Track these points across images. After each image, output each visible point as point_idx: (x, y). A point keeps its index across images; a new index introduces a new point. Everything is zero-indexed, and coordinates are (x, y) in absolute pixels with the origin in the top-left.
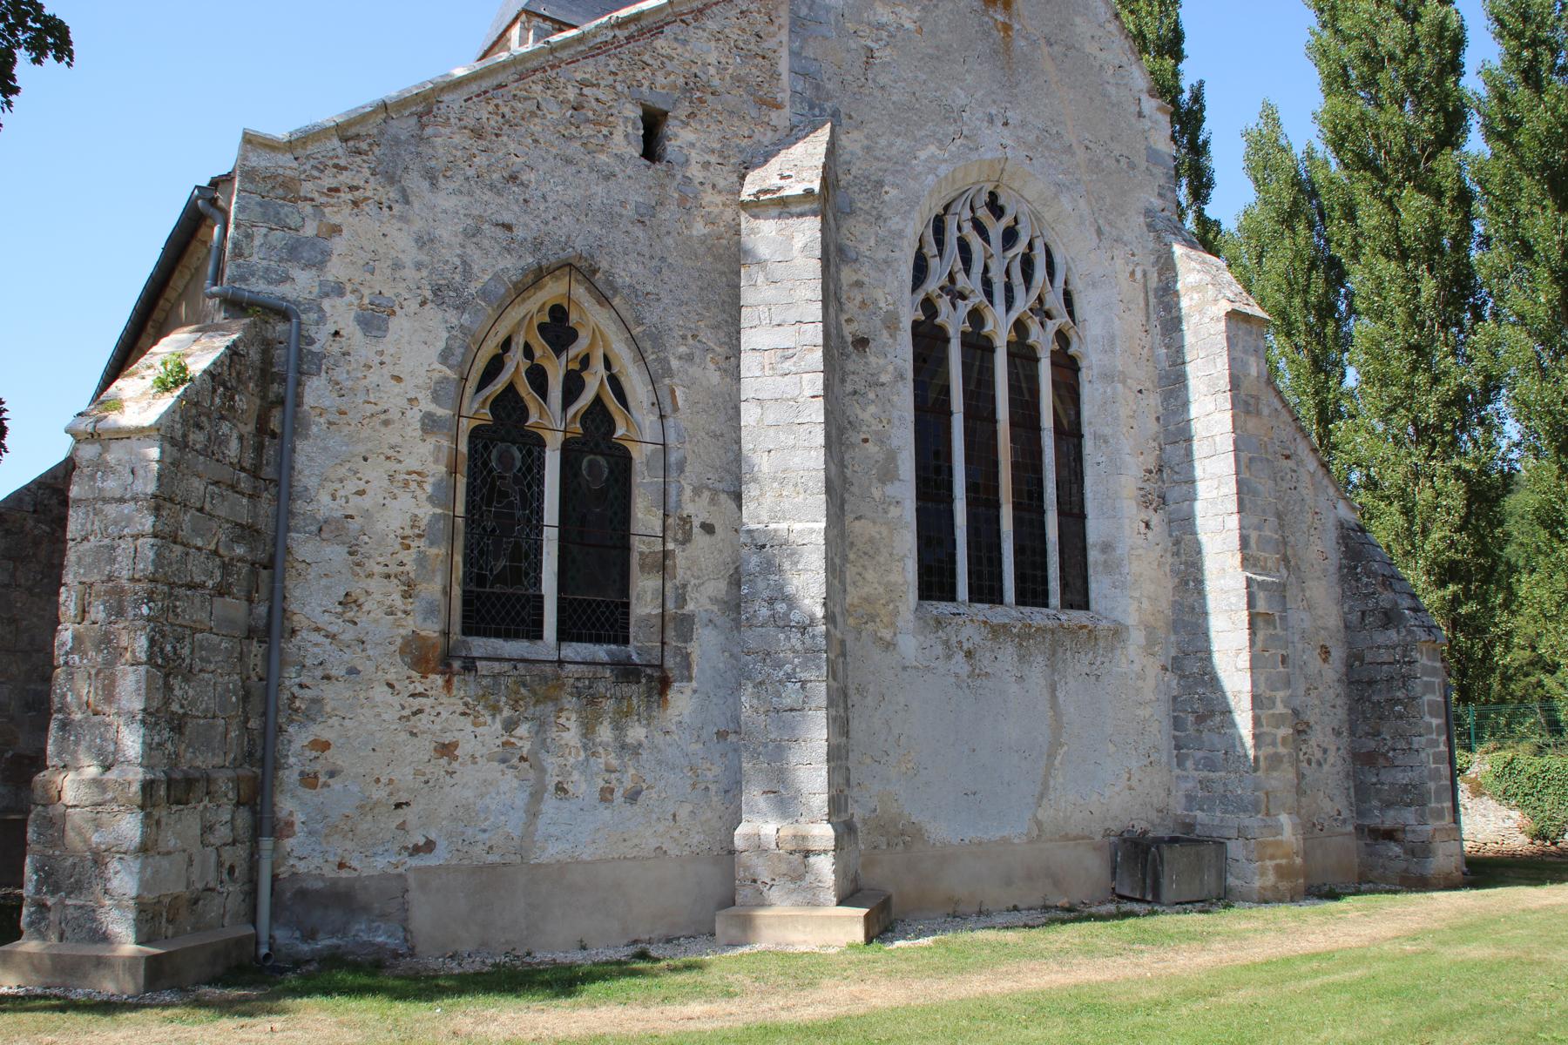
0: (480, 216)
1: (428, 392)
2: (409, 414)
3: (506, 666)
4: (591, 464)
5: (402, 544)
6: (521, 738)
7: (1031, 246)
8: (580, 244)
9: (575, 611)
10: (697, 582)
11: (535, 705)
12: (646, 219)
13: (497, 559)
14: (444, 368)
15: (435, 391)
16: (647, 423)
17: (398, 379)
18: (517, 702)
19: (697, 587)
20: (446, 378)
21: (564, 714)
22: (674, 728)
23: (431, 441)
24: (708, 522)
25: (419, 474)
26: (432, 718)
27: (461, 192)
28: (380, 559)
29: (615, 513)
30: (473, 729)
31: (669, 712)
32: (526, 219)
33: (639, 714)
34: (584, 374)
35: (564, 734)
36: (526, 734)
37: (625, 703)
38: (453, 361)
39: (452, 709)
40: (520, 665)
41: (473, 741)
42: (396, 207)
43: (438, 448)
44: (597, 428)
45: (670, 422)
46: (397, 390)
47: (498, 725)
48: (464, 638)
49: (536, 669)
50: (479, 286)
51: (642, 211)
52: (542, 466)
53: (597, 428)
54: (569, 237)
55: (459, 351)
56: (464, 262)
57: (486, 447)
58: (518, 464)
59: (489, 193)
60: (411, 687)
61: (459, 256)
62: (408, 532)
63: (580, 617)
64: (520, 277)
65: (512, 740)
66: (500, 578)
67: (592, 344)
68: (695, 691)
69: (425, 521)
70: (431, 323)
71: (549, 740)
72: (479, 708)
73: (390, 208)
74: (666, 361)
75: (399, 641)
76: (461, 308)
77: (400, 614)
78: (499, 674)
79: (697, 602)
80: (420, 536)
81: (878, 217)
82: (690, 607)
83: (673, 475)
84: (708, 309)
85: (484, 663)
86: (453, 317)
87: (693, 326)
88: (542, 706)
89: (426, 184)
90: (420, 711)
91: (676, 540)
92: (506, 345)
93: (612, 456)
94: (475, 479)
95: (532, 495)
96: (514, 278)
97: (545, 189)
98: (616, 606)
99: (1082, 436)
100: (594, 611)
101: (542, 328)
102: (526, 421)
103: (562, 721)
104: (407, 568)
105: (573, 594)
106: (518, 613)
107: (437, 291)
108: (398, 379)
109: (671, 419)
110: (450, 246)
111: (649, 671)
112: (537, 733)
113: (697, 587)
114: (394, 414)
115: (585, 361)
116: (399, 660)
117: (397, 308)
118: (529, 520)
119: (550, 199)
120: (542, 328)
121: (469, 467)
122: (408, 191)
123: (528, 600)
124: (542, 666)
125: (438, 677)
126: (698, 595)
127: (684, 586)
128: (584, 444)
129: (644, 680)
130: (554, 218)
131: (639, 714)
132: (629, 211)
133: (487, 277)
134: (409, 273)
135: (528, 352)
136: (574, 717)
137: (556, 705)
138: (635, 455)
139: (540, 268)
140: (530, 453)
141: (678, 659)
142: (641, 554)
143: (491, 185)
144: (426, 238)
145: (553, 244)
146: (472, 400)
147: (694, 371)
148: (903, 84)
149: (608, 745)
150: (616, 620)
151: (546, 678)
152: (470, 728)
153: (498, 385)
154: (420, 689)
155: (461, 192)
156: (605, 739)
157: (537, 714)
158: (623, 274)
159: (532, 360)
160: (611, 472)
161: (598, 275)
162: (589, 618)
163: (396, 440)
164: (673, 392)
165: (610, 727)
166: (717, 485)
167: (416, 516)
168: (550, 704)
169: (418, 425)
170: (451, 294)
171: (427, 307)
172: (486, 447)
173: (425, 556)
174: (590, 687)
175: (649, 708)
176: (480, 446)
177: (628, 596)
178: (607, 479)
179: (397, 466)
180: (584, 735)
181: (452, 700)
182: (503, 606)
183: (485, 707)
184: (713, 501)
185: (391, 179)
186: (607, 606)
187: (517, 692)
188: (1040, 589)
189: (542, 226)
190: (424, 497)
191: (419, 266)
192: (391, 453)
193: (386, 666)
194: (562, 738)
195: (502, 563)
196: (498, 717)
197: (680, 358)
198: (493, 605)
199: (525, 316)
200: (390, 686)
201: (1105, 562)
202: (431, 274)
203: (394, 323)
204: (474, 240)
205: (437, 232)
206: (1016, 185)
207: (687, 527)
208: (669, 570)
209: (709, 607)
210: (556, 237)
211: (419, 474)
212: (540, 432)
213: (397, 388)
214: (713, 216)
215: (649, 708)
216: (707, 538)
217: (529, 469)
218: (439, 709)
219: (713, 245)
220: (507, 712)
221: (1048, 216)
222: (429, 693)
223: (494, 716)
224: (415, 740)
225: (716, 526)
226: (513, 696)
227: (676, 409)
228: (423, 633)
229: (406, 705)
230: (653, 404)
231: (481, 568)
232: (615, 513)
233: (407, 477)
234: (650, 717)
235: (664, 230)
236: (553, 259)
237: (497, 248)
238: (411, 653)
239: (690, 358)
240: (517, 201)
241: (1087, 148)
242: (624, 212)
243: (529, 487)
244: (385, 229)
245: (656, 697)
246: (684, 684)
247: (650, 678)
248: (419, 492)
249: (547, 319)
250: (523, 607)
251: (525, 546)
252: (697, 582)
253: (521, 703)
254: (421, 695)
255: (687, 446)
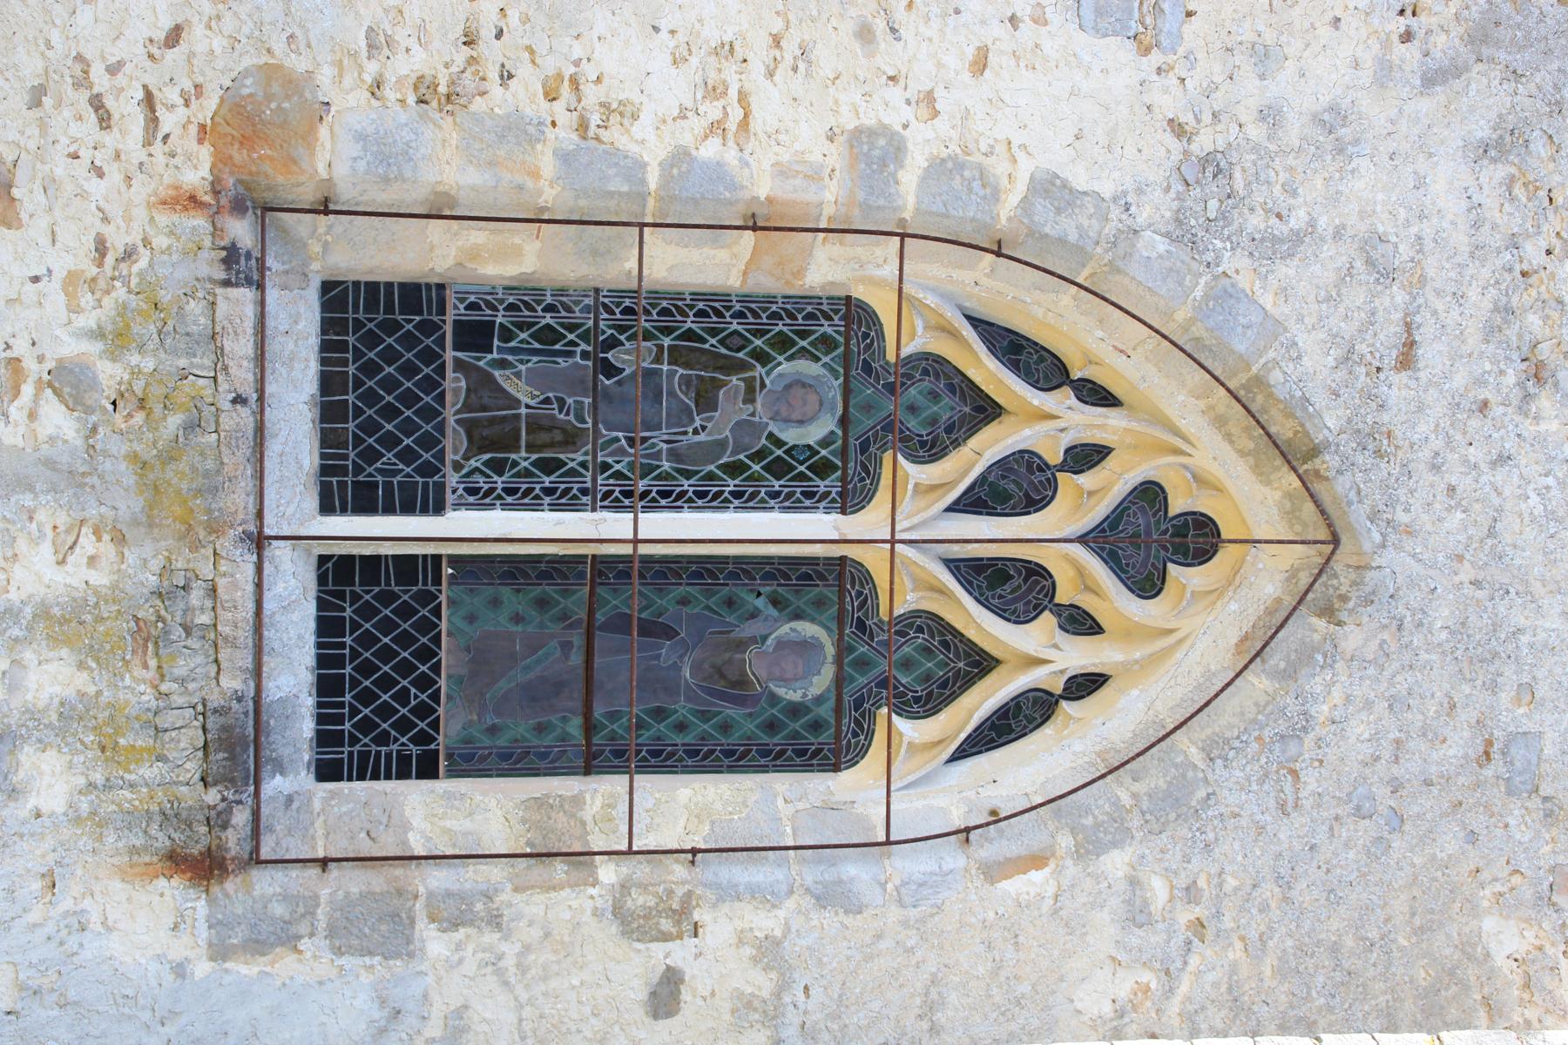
0: (1423, 281)
1: (954, 148)
2: (895, 94)
3: (243, 376)
4: (807, 647)
5: (559, 77)
6: (32, 416)
8: (1395, 563)
9: (405, 612)
10: (509, 962)
11: (133, 457)
12: (1496, 767)
13: (533, 379)
14: (1021, 188)
15: (961, 166)
16: (941, 802)
17: (980, 64)
18: (142, 403)
19: (495, 963)
20: (995, 195)
21: (107, 549)
22: (67, 904)
23: (835, 156)
24: (686, 995)
25: (744, 124)
26: (86, 154)
27: (1476, 225)
28: (514, 17)
29: (681, 727)
30: (59, 274)
31: (117, 885)
32: (1438, 409)
33: (108, 786)
34: (1047, 620)
36: (45, 428)
37: (143, 741)
38: (1043, 212)
40: (245, 416)
41: (22, 271)
42: (1411, 53)
43: (814, 176)
44: (907, 664)
45: (951, 857)
46: (951, 61)
47: (71, 347)
48: (315, 284)
49: (237, 461)
50: (1244, 281)
51: (1518, 752)
52: (792, 504)
54: (1410, 532)
55: (1067, 227)
56: (1297, 238)
57: (827, 343)
58: (791, 436)
61: (1312, 224)
62: (592, 95)
63: (387, 626)
64: (1280, 393)
65: (28, 390)
67: (1134, 633)
68: (180, 970)
69: (622, 142)
70: (1130, 151)
71: (27, 500)
72: (120, 292)
73: (1407, 37)
74: (1121, 837)
75: (298, 64)
76: (1182, 234)
77: (371, 68)
78: (220, 352)
80: (582, 127)
82: (435, 943)
83: (808, 871)
86: (1154, 209)
87: (1228, 922)
88: (130, 480)
89: (1482, 130)
90: (105, 121)
91: (625, 887)
92: (1097, 395)
93: (838, 710)
95: (710, 476)
96: (1276, 377)
97: (1527, 461)
98: (424, 738)
100: (405, 668)
101: (1150, 494)
102: (907, 457)
103: (87, 543)
104: (496, 90)
106: (390, 441)
107: (1214, 166)
108: (980, 64)
110: (1335, 199)
111: (241, 817)
112: (50, 464)
113: (495, 963)
114: (889, 56)
115: (1081, 623)
116: (247, 62)
117: (1156, 58)
119: (1500, 476)
120: (1150, 494)
122: (1458, 84)
123: (429, 470)
124: (246, 483)
125: (205, 171)
126: (470, 967)
127: (495, 921)
128: (861, 626)
129: (212, 796)
130: (1452, 489)
131: (108, 786)
132: (1510, 715)
133: (1267, 301)
134: (1249, 93)
135: (1086, 457)
136: (100, 579)
137: (135, 523)
139: (1314, 452)
140: (823, 469)
141: (278, 910)
142: (578, 801)
143: (1509, 311)
144: (1345, 132)
147: (1104, 929)
151: (214, 491)
152: (62, 264)
153: (988, 371)
155: (1476, 225)
158: (1337, 695)
159: (1062, 467)
160: (795, 710)
161: (1321, 624)
162: (386, 654)
163: (826, 60)
164: (1037, 861)
165: (70, 693)
166: (793, 1017)
167: (635, 117)
169: (869, 121)
170: (1213, 204)
171: (1170, 140)
172: (827, 343)
173: (533, 141)
174: (188, 630)
178: (774, 699)
179: (757, 67)
180: (43, 613)
181: (140, 213)
182: (409, 399)
183: (123, 309)
184: (745, 1004)
185: (1480, 37)
186: (424, 711)
187: (168, 404)
189: (1425, 454)
190: (687, 139)
191: (1270, 115)
192: (790, 47)
193: (229, 24)
194: (35, 542)
195: (523, 393)
196: (95, 348)
197: (1134, 882)
198: (409, 370)
199: (1177, 433)
200: (174, 36)
202: (1256, 148)
203: (1118, 51)
204: (1359, 265)
207: (666, 925)
208: (537, 871)
209: (437, 1011)
211: (744, 124)
212: (883, 496)
213: (956, 62)
214: (1548, 980)
216: (638, 992)
217: (778, 468)
218: (114, 175)
219: (1466, 988)
220: (110, 374)
222: (158, 147)
223: (98, 334)
224: (20, 101)
225: (674, 1023)
226: (157, 391)
227: (994, 872)
228: (323, 132)
229: (121, 80)
230: (993, 813)
231: (507, 335)
232: (681, 727)
233: (733, 93)
235: (1478, 821)
237: (1348, 329)
238: (269, 98)
239: (1137, 915)
240: (1480, 382)
242: (1505, 698)
244: (1350, 22)
245: (162, 842)
246: (203, 933)
247: (219, 820)
248: (697, 125)
249: (1177, 505)
250: (407, 456)
252: (509, 962)
253: (139, 418)
254: (153, 121)
255: (894, 914)
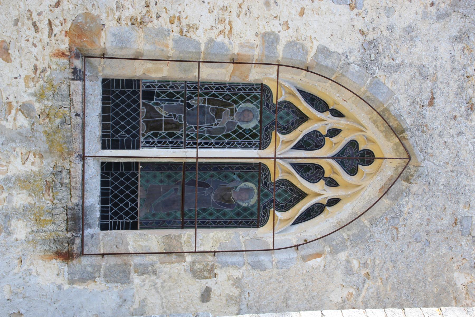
0: (437, 79)
1: (294, 39)
2: (276, 22)
3: (78, 107)
4: (249, 190)
5: (174, 17)
6: (15, 119)
8: (428, 165)
9: (128, 179)
10: (159, 285)
11: (45, 132)
12: (458, 227)
13: (166, 108)
14: (314, 51)
15: (296, 44)
16: (290, 237)
17: (302, 13)
19: (154, 285)
20: (307, 53)
21: (37, 160)
22: (25, 267)
23: (258, 41)
24: (212, 295)
25: (230, 31)
26: (31, 40)
29: (211, 214)
30: (23, 76)
31: (40, 261)
33: (38, 232)
34: (322, 182)
35: (19, 160)
36: (19, 123)
37: (48, 218)
39: (39, 57)
40: (79, 120)
41: (11, 76)
42: (433, 10)
43: (252, 47)
44: (279, 195)
45: (293, 254)
46: (293, 12)
47: (26, 99)
48: (100, 79)
49: (77, 133)
50: (382, 79)
51: (465, 223)
52: (244, 147)
53: (279, 195)
54: (432, 156)
55: (328, 62)
56: (398, 66)
57: (255, 98)
58: (244, 126)
59: (456, 86)
60: (57, 22)
61: (403, 62)
62: (184, 22)
63: (122, 183)
64: (393, 113)
65: (13, 111)
66: (151, 110)
67: (348, 186)
68: (59, 287)
69: (193, 37)
70: (348, 39)
71: (13, 145)
72: (41, 82)
75: (95, 13)
77: (117, 14)
78: (71, 100)
79: (142, 286)
80: (181, 32)
82: (136, 279)
83: (249, 258)
84: (393, 289)
85: (80, 88)
86: (355, 57)
87: (376, 274)
88: (44, 139)
89: (455, 33)
90: (37, 30)
91: (194, 263)
92: (337, 114)
93: (258, 209)
94: (229, 89)
95: (220, 138)
96: (392, 108)
98: (133, 217)
100: (127, 196)
101: (353, 144)
103: (32, 158)
104: (155, 21)
105: (141, 176)
106: (123, 127)
107: (373, 44)
108: (302, 13)
109: (296, 255)
110: (410, 54)
111: (78, 241)
112: (20, 134)
114: (274, 10)
115: (332, 183)
116: (80, 12)
117: (356, 11)
118: (200, 137)
119: (460, 138)
120: (353, 144)
121: (238, 84)
122: (448, 19)
123: (135, 136)
124: (79, 140)
125: (67, 45)
126: (147, 287)
127: (155, 273)
128: (266, 184)
129: (69, 235)
130: (445, 143)
131: (38, 232)
132: (462, 211)
133: (389, 85)
134: (384, 22)
135: (334, 132)
136: (35, 169)
137: (46, 152)
138: (261, 229)
139: (403, 131)
140: (254, 136)
141: (89, 269)
142: (180, 236)
145: (425, 141)
146: (292, 84)
147: (339, 276)
149: (9, 202)
150: (121, 217)
152: (24, 73)
154: (56, 30)
155: (453, 62)
156: (15, 199)
157: (38, 135)
158: (410, 205)
159: (327, 136)
160: (245, 209)
161: (405, 183)
162: (122, 192)
163: (255, 12)
164: (319, 255)
165: (26, 203)
166: (245, 302)
167: (197, 29)
168: (46, 146)
169: (268, 30)
170: (373, 56)
171: (360, 36)
172: (255, 98)
173: (166, 36)
174: (62, 184)
175: (44, 242)
176: (255, 93)
177: (142, 228)
178: (239, 206)
179: (234, 14)
180: (18, 179)
181: (47, 58)
182: (129, 114)
183: (42, 87)
186: (133, 209)
189: (437, 132)
190: (213, 36)
191: (390, 29)
192: (244, 8)
194: (16, 157)
197: (348, 262)
198: (129, 106)
199: (362, 125)
202: (386, 39)
204: (417, 74)
205: (419, 43)
207: (206, 274)
208: (167, 258)
210: (430, 143)
211: (230, 31)
213: (295, 12)
215: (44, 242)
218: (40, 46)
219: (448, 294)
220: (38, 107)
223: (35, 95)
224: (11, 24)
226: (53, 112)
227: (306, 258)
228: (103, 33)
231: (158, 95)
232: (211, 214)
233: (227, 22)
234: (35, 242)
235: (453, 243)
236: (412, 141)
237: (414, 94)
239: (349, 271)
240: (454, 110)
242: (461, 206)
243: (227, 136)
245: (54, 248)
246: (67, 276)
247: (71, 242)
248: (216, 31)
249: (361, 147)
250: (128, 132)
251: (178, 133)
252: (159, 285)
253: (47, 120)
254: (51, 30)
255: (275, 271)
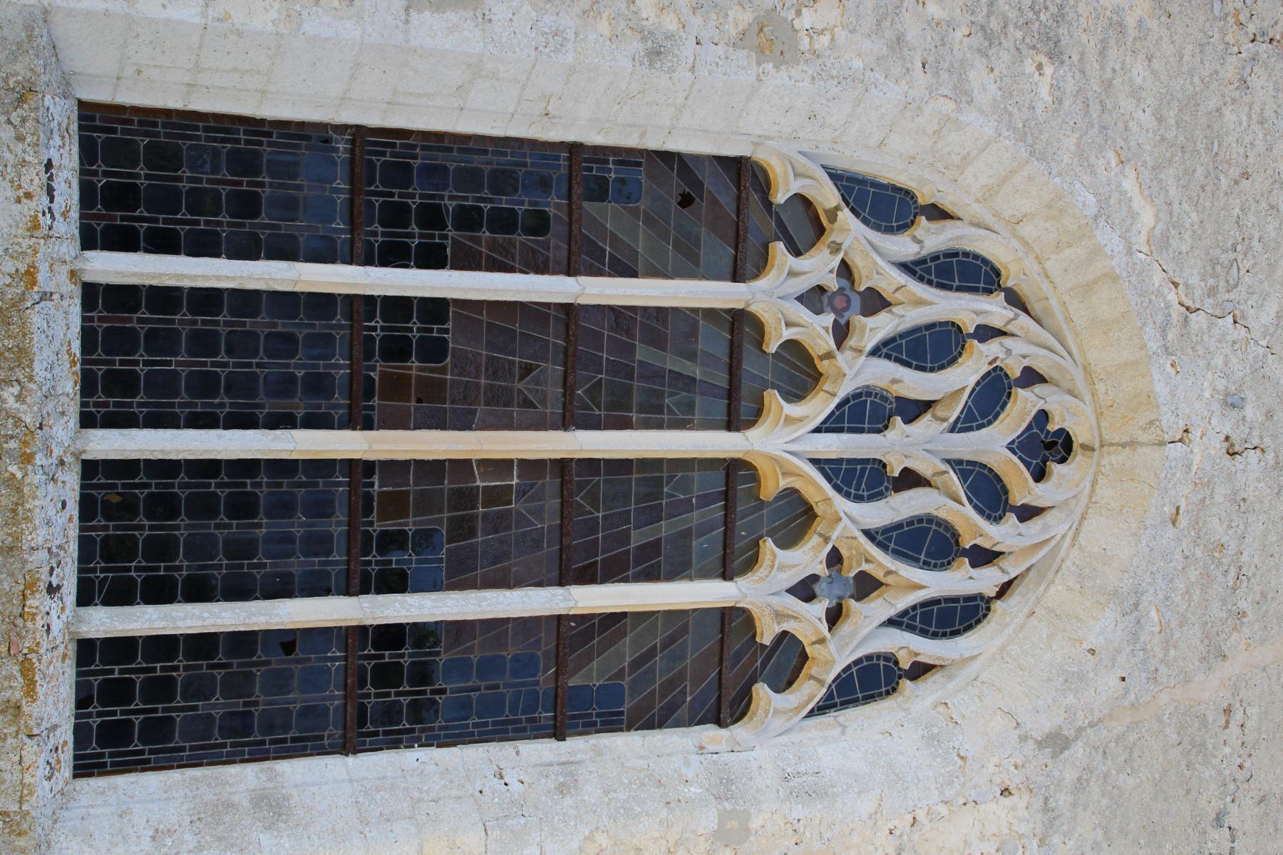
7: (983, 557)
81: (990, 37)
99: (560, 736)
148: (1260, 146)
188: (136, 571)
201: (230, 806)
206: (1106, 493)
221: (1058, 592)
241: (1228, 711)
